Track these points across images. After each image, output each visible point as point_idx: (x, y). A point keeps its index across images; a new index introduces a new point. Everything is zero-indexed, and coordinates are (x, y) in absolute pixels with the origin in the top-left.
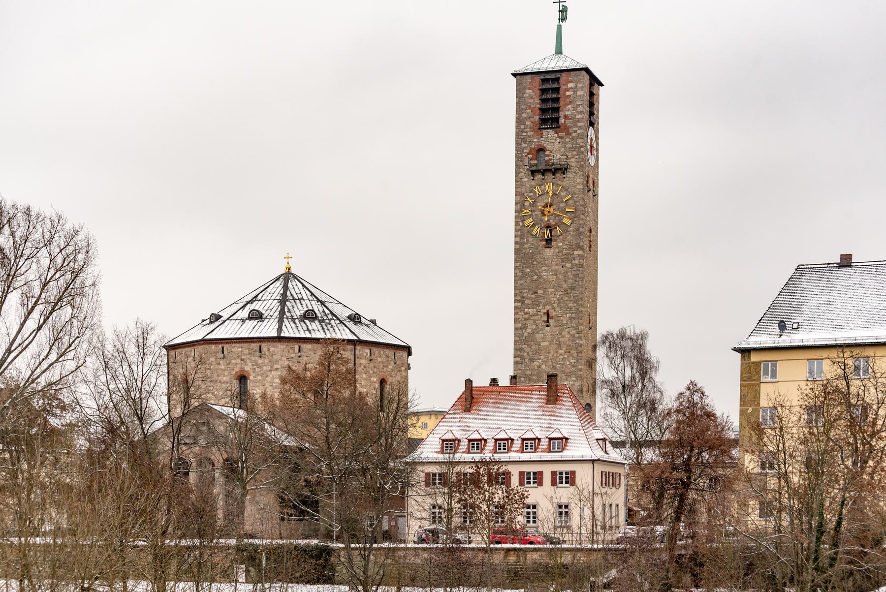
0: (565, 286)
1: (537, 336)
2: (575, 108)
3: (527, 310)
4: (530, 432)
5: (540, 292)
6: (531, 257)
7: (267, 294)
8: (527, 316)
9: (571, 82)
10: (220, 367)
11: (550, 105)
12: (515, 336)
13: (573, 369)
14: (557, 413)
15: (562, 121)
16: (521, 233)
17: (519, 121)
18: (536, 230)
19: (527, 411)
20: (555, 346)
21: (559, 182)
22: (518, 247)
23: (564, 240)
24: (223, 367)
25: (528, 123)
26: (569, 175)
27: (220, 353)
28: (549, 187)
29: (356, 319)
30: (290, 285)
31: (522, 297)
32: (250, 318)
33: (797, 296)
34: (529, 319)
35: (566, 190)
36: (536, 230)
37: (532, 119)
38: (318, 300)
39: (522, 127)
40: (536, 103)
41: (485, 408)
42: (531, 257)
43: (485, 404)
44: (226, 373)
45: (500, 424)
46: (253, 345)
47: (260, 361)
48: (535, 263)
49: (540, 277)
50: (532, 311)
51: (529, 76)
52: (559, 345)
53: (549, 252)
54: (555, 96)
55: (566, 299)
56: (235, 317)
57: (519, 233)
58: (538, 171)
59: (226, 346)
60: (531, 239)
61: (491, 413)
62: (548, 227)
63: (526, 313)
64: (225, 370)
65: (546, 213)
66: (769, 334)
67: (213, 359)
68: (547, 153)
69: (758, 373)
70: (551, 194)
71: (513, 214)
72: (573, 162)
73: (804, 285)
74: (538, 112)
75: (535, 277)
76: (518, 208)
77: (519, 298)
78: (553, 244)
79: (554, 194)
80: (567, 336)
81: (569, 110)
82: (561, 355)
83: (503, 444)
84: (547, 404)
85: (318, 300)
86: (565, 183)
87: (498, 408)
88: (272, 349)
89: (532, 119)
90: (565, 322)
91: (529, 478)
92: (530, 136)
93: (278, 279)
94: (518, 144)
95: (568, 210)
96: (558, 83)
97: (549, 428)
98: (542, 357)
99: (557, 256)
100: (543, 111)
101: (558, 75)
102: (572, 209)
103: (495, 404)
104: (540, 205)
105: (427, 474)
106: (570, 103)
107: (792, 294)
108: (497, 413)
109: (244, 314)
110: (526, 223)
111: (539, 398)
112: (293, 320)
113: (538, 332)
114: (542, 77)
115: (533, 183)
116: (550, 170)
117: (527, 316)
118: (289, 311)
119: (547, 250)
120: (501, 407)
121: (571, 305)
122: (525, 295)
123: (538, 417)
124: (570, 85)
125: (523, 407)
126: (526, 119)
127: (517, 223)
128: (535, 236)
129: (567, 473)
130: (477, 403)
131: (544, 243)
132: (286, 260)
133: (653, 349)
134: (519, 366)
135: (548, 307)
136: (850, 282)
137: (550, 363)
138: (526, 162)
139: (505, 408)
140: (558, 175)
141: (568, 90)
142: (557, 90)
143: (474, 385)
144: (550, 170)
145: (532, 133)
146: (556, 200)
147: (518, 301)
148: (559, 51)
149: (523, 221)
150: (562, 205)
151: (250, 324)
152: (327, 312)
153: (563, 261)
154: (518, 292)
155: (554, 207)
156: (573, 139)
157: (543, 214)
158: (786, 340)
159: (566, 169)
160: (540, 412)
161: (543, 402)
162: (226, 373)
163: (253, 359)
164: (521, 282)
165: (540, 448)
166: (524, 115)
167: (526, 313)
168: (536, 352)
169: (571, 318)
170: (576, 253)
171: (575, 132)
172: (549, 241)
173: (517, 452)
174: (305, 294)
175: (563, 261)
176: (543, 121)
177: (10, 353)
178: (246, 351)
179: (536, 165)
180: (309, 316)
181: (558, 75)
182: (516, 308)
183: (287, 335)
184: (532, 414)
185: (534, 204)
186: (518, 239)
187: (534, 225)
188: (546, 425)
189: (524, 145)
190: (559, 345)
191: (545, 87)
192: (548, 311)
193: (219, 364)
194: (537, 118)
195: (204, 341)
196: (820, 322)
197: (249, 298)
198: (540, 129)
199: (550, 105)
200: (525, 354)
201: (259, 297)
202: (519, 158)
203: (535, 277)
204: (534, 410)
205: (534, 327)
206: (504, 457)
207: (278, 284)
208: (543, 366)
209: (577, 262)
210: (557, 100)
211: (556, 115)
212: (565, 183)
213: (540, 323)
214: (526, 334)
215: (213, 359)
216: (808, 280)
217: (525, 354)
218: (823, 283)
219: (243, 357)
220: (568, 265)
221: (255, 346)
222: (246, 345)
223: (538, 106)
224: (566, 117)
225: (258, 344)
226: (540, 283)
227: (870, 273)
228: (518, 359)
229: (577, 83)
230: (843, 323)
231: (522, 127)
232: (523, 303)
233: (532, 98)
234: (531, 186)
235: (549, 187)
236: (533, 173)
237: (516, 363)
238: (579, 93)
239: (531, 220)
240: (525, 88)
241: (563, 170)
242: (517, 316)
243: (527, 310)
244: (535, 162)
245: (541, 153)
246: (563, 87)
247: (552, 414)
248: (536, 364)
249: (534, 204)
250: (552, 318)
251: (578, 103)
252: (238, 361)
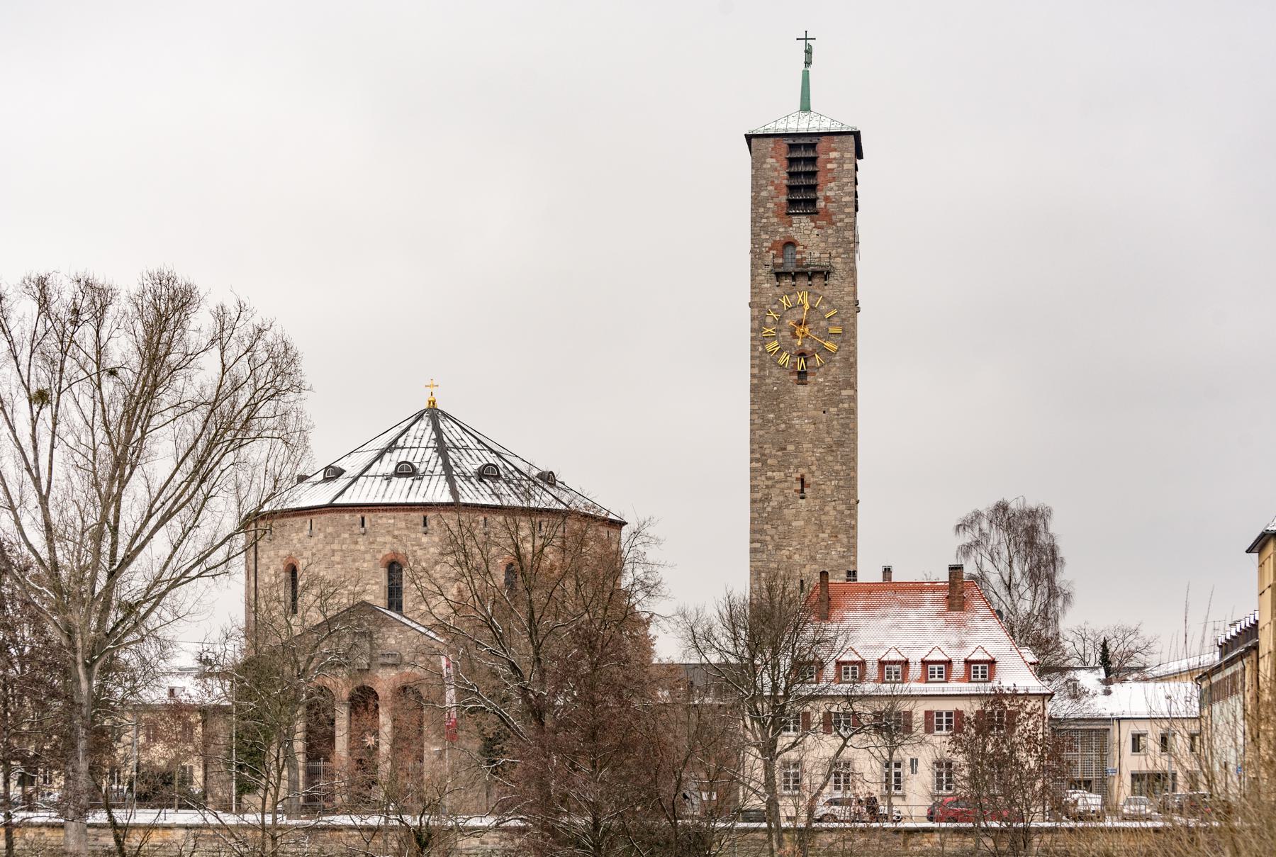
0: (828, 439)
1: (786, 511)
2: (841, 188)
3: (770, 474)
4: (936, 652)
5: (791, 448)
6: (777, 397)
7: (410, 439)
8: (770, 483)
9: (835, 150)
10: (358, 547)
11: (803, 181)
12: (752, 512)
13: (842, 561)
14: (969, 623)
15: (821, 204)
16: (761, 361)
17: (756, 202)
18: (784, 359)
19: (920, 620)
20: (814, 527)
21: (818, 291)
22: (756, 381)
24: (362, 548)
25: (770, 205)
26: (832, 281)
27: (359, 526)
28: (804, 298)
30: (442, 426)
31: (763, 455)
32: (398, 474)
34: (773, 486)
35: (829, 303)
36: (784, 359)
37: (776, 200)
38: (492, 451)
39: (761, 210)
40: (782, 177)
41: (851, 614)
42: (777, 397)
43: (849, 610)
44: (368, 557)
45: (881, 639)
46: (413, 514)
47: (424, 539)
48: (782, 405)
49: (791, 426)
50: (778, 475)
51: (772, 140)
52: (821, 527)
53: (803, 391)
54: (810, 168)
55: (830, 458)
57: (757, 362)
58: (787, 274)
59: (368, 516)
60: (775, 371)
61: (862, 622)
62: (802, 354)
63: (768, 479)
64: (366, 552)
65: (798, 333)
67: (346, 536)
68: (799, 248)
70: (807, 307)
71: (748, 335)
72: (838, 263)
74: (785, 190)
75: (783, 426)
76: (756, 325)
77: (758, 456)
78: (809, 378)
79: (812, 308)
80: (833, 513)
81: (831, 189)
82: (823, 540)
83: (895, 669)
84: (949, 610)
85: (492, 451)
86: (827, 292)
87: (873, 615)
89: (776, 200)
90: (828, 492)
91: (940, 721)
92: (773, 224)
93: (419, 417)
94: (755, 236)
95: (831, 330)
96: (814, 150)
98: (794, 543)
99: (816, 397)
100: (791, 189)
101: (814, 140)
102: (839, 330)
103: (866, 608)
104: (790, 322)
106: (834, 179)
108: (873, 623)
109: (388, 465)
110: (769, 348)
111: (935, 602)
112: (468, 478)
113: (787, 507)
114: (791, 142)
115: (778, 290)
116: (804, 274)
117: (770, 483)
118: (456, 465)
119: (801, 387)
120: (877, 613)
121: (838, 467)
122: (767, 451)
123: (940, 630)
124: (833, 155)
125: (912, 614)
127: (753, 348)
128: (782, 367)
131: (796, 377)
132: (429, 390)
134: (759, 556)
135: (802, 470)
137: (806, 552)
138: (769, 259)
139: (884, 616)
140: (816, 281)
141: (830, 161)
142: (813, 160)
144: (804, 274)
145: (776, 220)
147: (757, 460)
148: (805, 107)
149: (763, 345)
150: (823, 324)
151: (401, 484)
152: (511, 468)
153: (825, 405)
154: (756, 446)
155: (811, 326)
156: (838, 231)
157: (795, 336)
159: (828, 273)
160: (941, 622)
161: (942, 607)
162: (368, 557)
163: (413, 536)
164: (761, 433)
165: (954, 675)
166: (764, 194)
167: (768, 479)
168: (785, 536)
169: (837, 487)
170: (844, 393)
171: (841, 220)
172: (802, 375)
174: (469, 441)
175: (825, 405)
176: (792, 203)
177: (150, 516)
178: (403, 525)
179: (782, 265)
180: (486, 474)
181: (814, 140)
182: (752, 470)
183: (468, 501)
184: (928, 624)
185: (780, 322)
186: (756, 371)
187: (781, 352)
188: (954, 641)
189: (764, 236)
190: (821, 527)
191: (794, 155)
192: (803, 476)
193: (356, 543)
194: (783, 199)
195: (332, 508)
197: (383, 442)
198: (788, 214)
199: (803, 181)
200: (768, 538)
201: (400, 442)
202: (756, 255)
203: (783, 426)
204: (930, 618)
205: (781, 498)
206: (900, 688)
207: (423, 424)
208: (796, 557)
209: (846, 406)
211: (812, 196)
212: (826, 293)
214: (769, 509)
215: (346, 536)
217: (768, 538)
219: (396, 533)
220: (833, 410)
221: (417, 516)
222: (402, 514)
223: (785, 182)
224: (827, 199)
225: (421, 514)
226: (790, 435)
228: (758, 545)
231: (761, 210)
233: (776, 170)
234: (775, 295)
235: (804, 298)
236: (779, 275)
237: (753, 551)
238: (846, 167)
239: (776, 343)
240: (764, 156)
241: (825, 274)
242: (755, 483)
243: (770, 474)
244: (780, 261)
245: (790, 250)
246: (822, 157)
249: (780, 322)
250: (809, 486)
251: (845, 180)
252: (389, 539)
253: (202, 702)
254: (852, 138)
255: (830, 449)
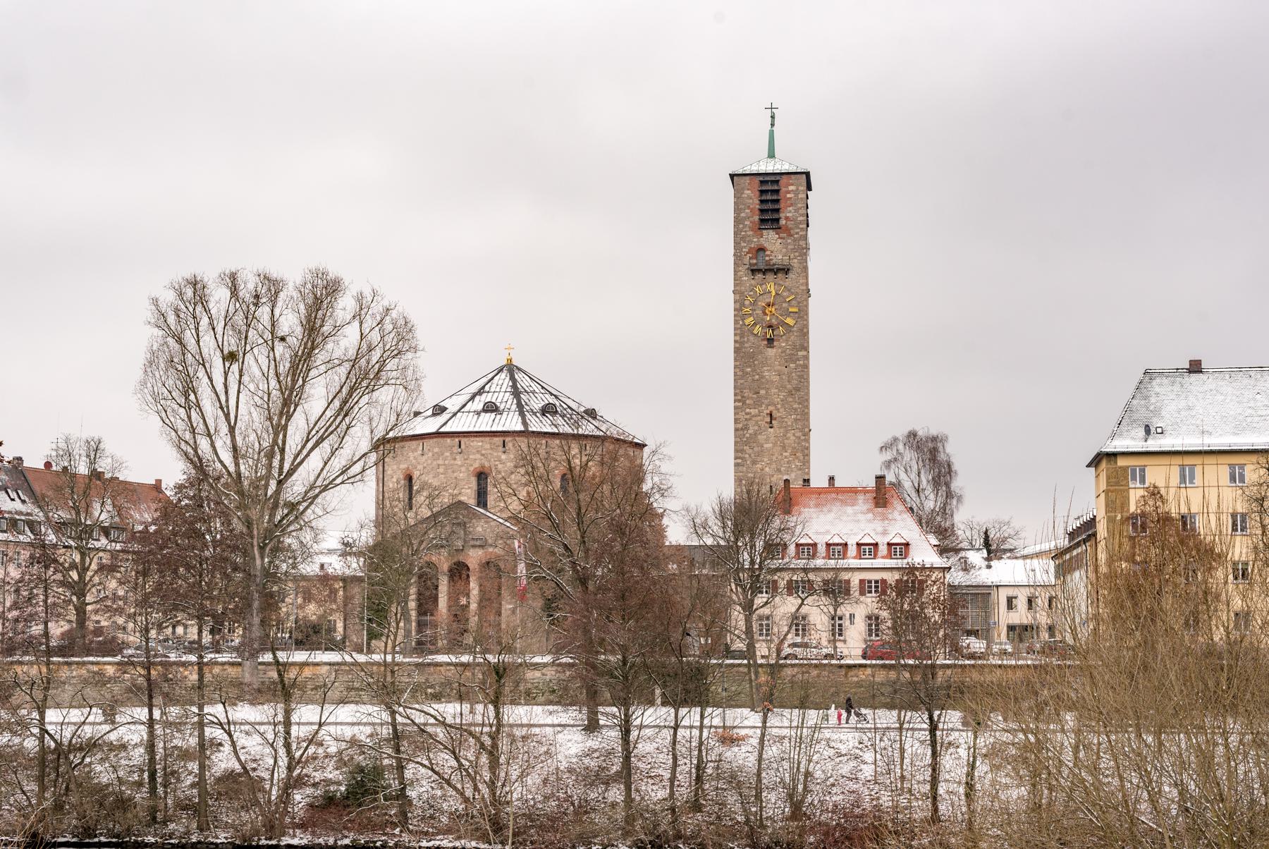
5: (763, 392)
6: (752, 356)
11: (770, 206)
14: (890, 517)
15: (783, 222)
16: (741, 332)
17: (738, 221)
18: (757, 329)
19: (855, 514)
23: (787, 341)
26: (791, 275)
28: (771, 287)
29: (592, 414)
33: (1153, 400)
36: (757, 329)
42: (752, 356)
44: (463, 469)
45: (828, 528)
47: (503, 457)
49: (763, 377)
50: (754, 411)
52: (784, 448)
54: (775, 197)
56: (466, 409)
58: (759, 271)
59: (464, 441)
60: (751, 338)
62: (770, 326)
66: (1133, 438)
69: (1126, 478)
71: (732, 313)
72: (795, 263)
73: (1157, 389)
86: (788, 283)
93: (501, 370)
94: (736, 244)
97: (885, 533)
102: (795, 310)
103: (817, 506)
105: (862, 581)
106: (791, 205)
107: (1146, 398)
108: (822, 516)
109: (478, 404)
110: (747, 322)
111: (866, 501)
112: (535, 414)
116: (770, 270)
121: (796, 406)
123: (869, 521)
124: (791, 188)
125: (849, 510)
126: (745, 219)
127: (736, 322)
129: (876, 582)
130: (798, 504)
133: (954, 451)
135: (771, 408)
136: (1205, 388)
137: (774, 466)
139: (830, 511)
141: (789, 192)
142: (777, 192)
144: (770, 270)
146: (779, 300)
148: (771, 155)
156: (795, 240)
157: (765, 314)
158: (1154, 444)
160: (870, 516)
161: (871, 505)
165: (880, 554)
169: (796, 420)
172: (770, 341)
173: (855, 558)
177: (308, 440)
178: (488, 446)
180: (548, 410)
182: (736, 408)
184: (861, 517)
185: (754, 303)
187: (755, 324)
188: (880, 529)
190: (784, 448)
191: (764, 188)
194: (757, 218)
195: (438, 434)
196: (1185, 428)
197: (475, 388)
199: (770, 206)
201: (487, 388)
202: (738, 258)
204: (862, 513)
206: (842, 563)
207: (503, 375)
210: (777, 201)
213: (762, 424)
216: (1160, 385)
218: (1177, 388)
220: (792, 365)
221: (498, 440)
222: (487, 439)
224: (787, 218)
227: (1223, 379)
229: (797, 186)
230: (1210, 429)
232: (744, 403)
235: (771, 287)
237: (736, 465)
245: (761, 254)
246: (783, 189)
247: (884, 518)
249: (754, 303)
252: (478, 456)
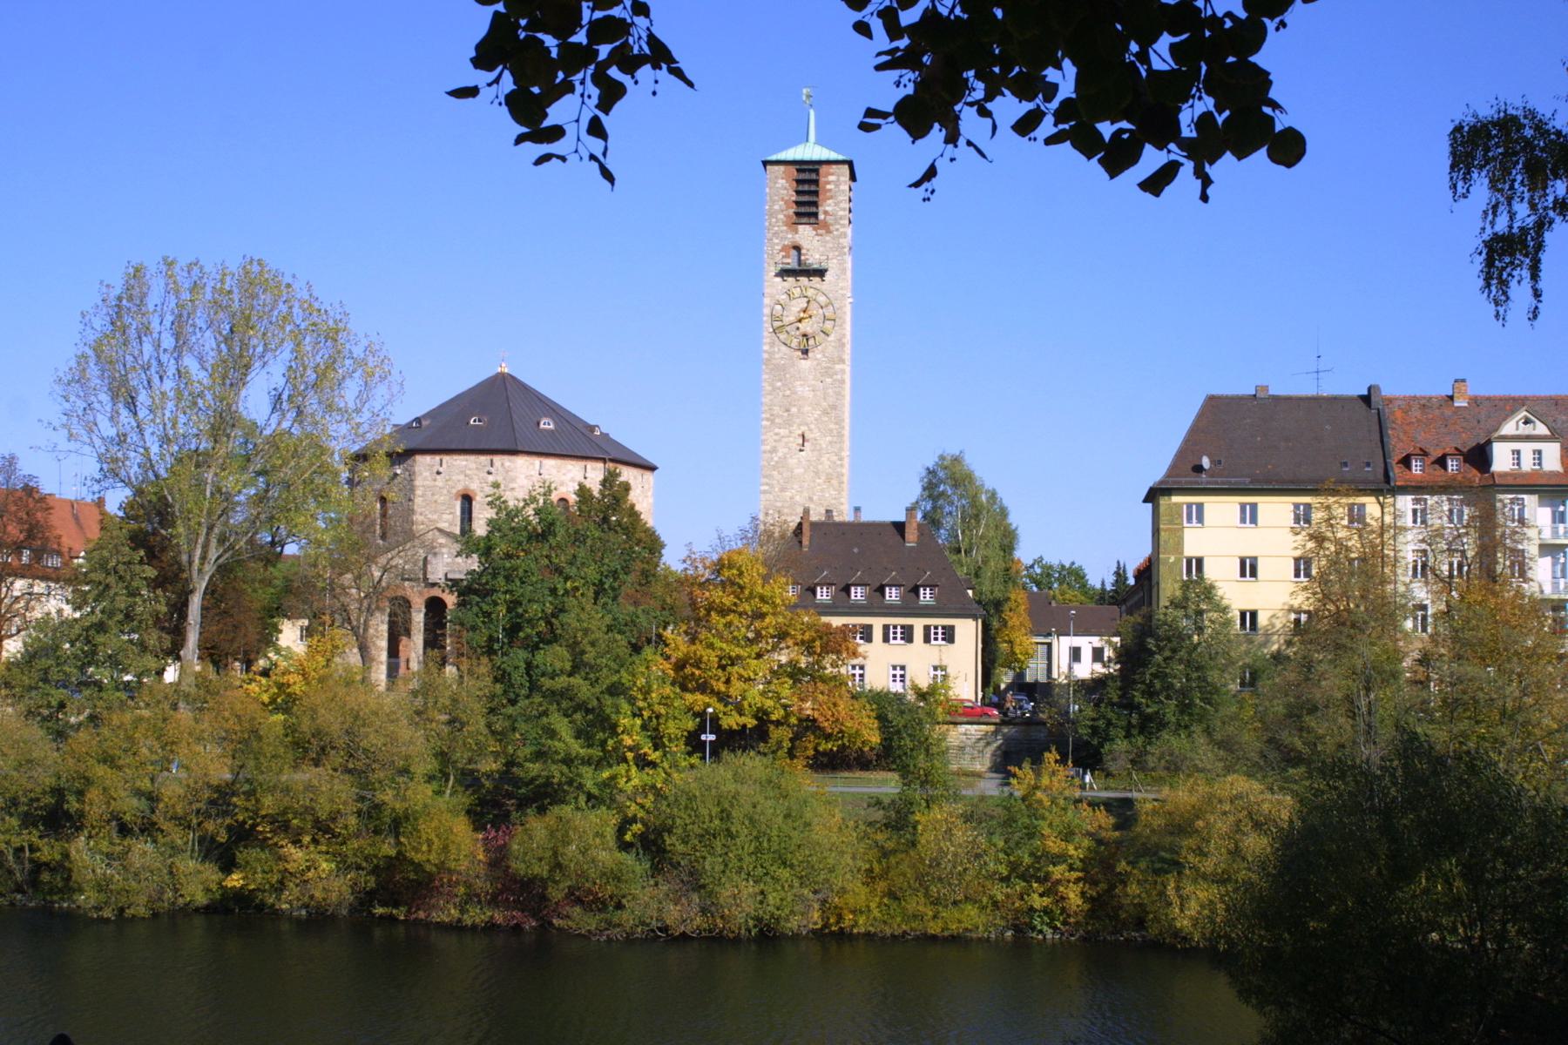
5: (794, 410)
15: (821, 217)
26: (828, 277)
50: (782, 432)
53: (805, 364)
88: (507, 464)
103: (246, 847)
124: (831, 178)
135: (804, 428)
137: (806, 494)
143: (1025, 554)
172: (805, 352)
178: (474, 466)
190: (817, 473)
194: (791, 211)
220: (829, 380)
224: (826, 213)
232: (773, 422)
246: (822, 180)
248: (789, 494)
252: (462, 477)
253: (1541, 504)
254: (845, 169)
255: (825, 413)
